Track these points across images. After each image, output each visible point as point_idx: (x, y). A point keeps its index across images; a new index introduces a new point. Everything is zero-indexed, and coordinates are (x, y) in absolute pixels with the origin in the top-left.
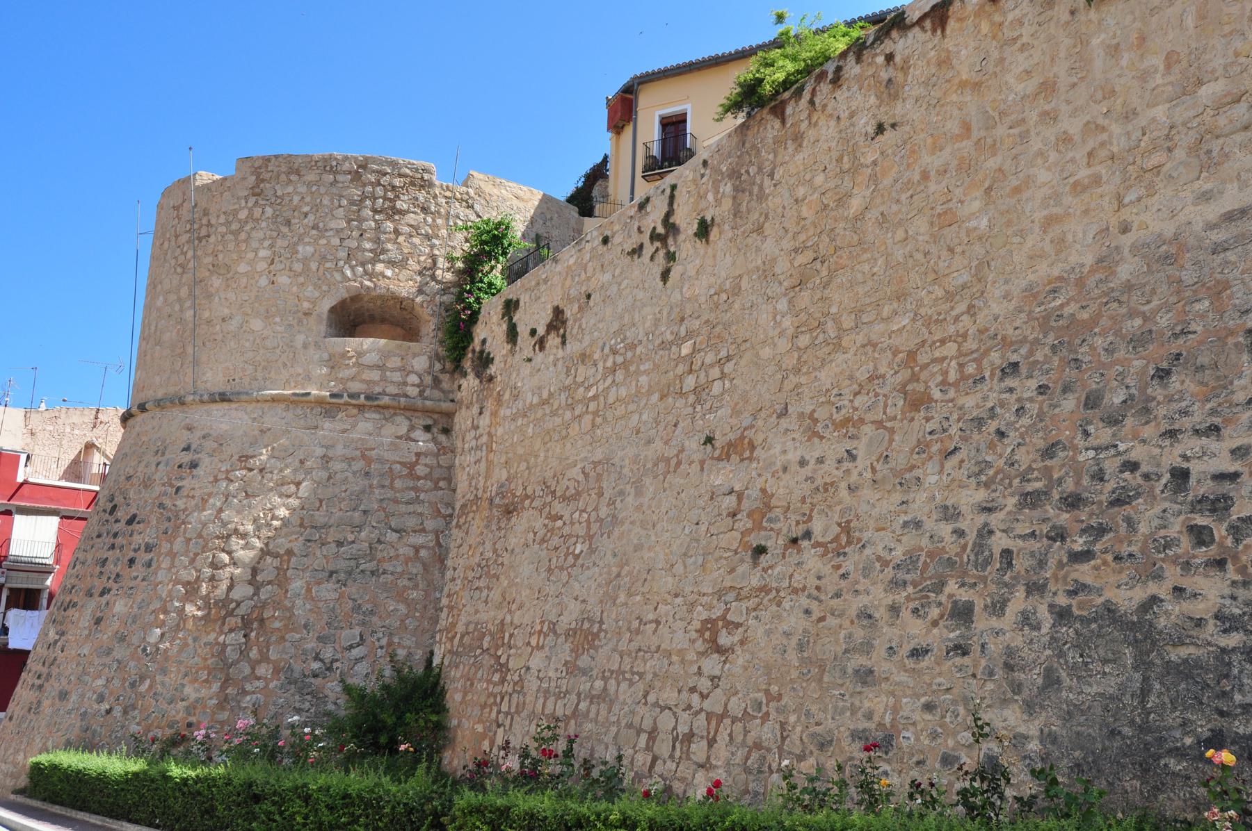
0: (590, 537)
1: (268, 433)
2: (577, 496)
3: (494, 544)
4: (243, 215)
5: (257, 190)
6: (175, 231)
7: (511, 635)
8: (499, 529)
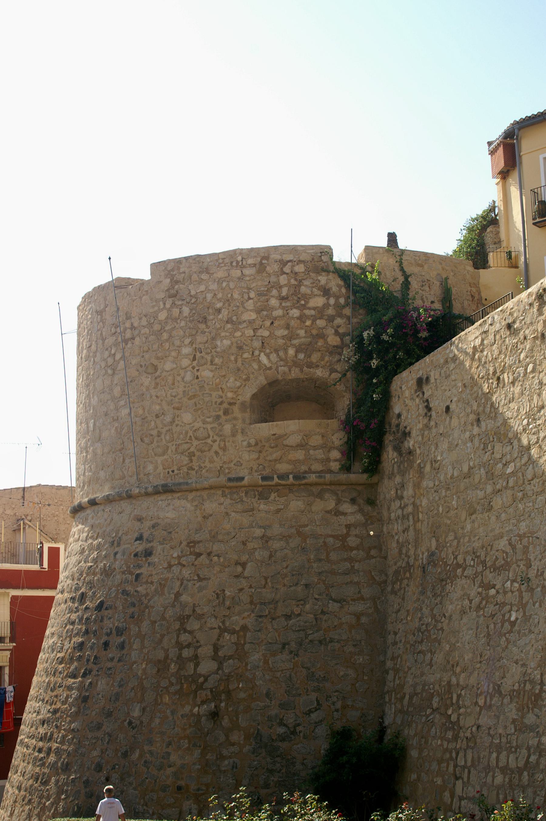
0: (522, 606)
1: (211, 518)
2: (506, 566)
3: (432, 610)
4: (162, 316)
5: (172, 292)
6: (101, 334)
7: (459, 696)
8: (435, 595)
